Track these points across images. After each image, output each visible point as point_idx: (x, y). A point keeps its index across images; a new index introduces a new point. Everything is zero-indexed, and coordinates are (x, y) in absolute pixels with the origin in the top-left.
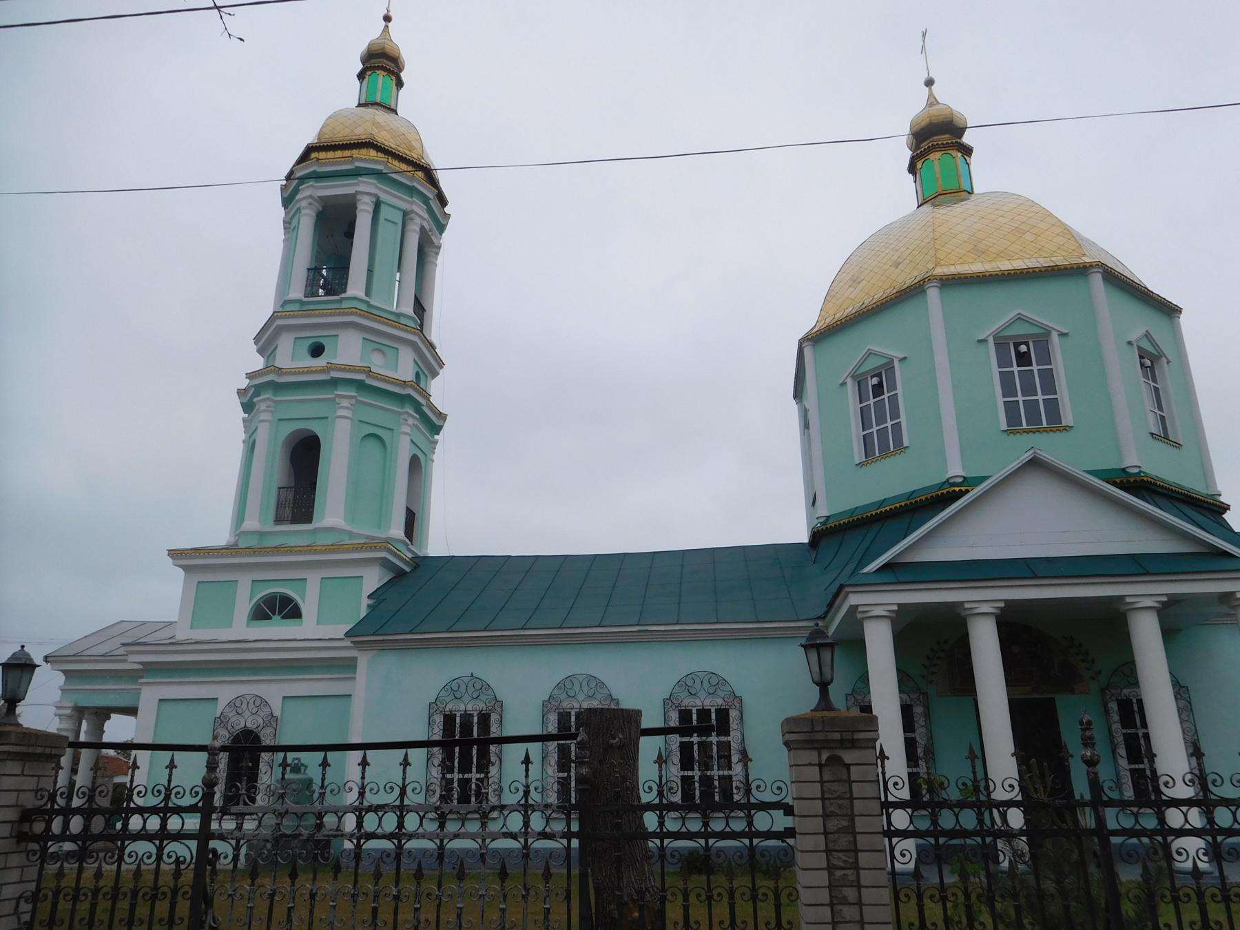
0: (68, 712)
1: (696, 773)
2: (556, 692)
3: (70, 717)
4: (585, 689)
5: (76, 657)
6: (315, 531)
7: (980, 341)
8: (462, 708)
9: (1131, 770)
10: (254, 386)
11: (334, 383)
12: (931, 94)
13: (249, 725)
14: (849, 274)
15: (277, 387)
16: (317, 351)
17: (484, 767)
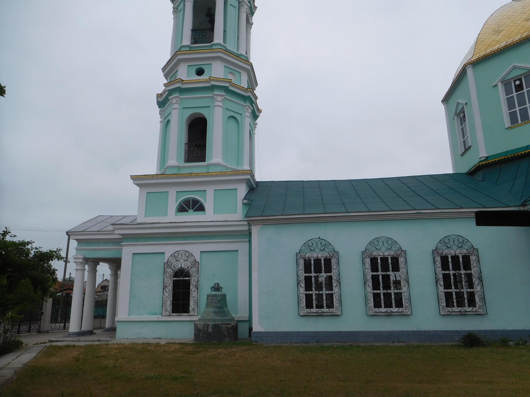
0: (81, 260)
1: (453, 290)
2: (369, 247)
3: (81, 263)
4: (386, 245)
5: (83, 232)
6: (208, 166)
7: (494, 86)
8: (315, 255)
9: (306, 295)
10: (167, 91)
11: (212, 88)
13: (183, 266)
14: (492, 27)
15: (181, 91)
16: (200, 72)
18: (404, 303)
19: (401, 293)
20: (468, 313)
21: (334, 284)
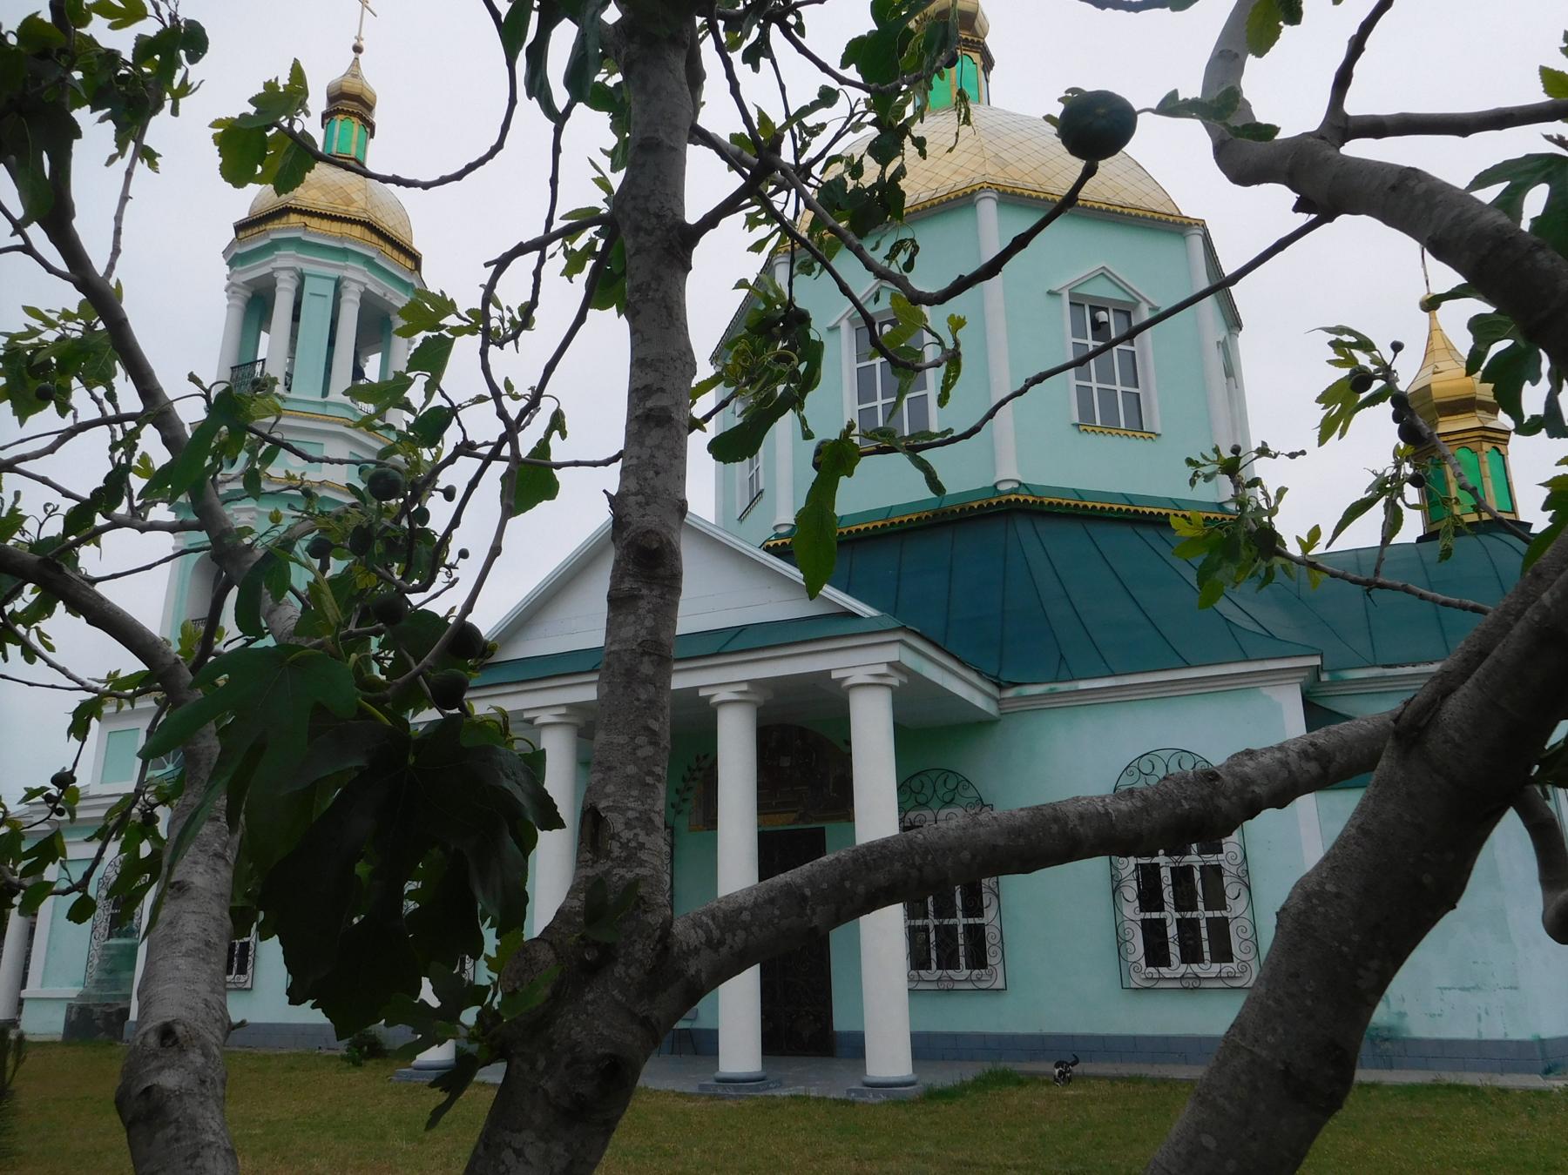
2: (971, 793)
7: (1051, 293)
9: (1143, 921)
12: (1434, 329)
17: (974, 906)
18: (1235, 949)
19: (1226, 919)
20: (1161, 984)
21: (1231, 892)
